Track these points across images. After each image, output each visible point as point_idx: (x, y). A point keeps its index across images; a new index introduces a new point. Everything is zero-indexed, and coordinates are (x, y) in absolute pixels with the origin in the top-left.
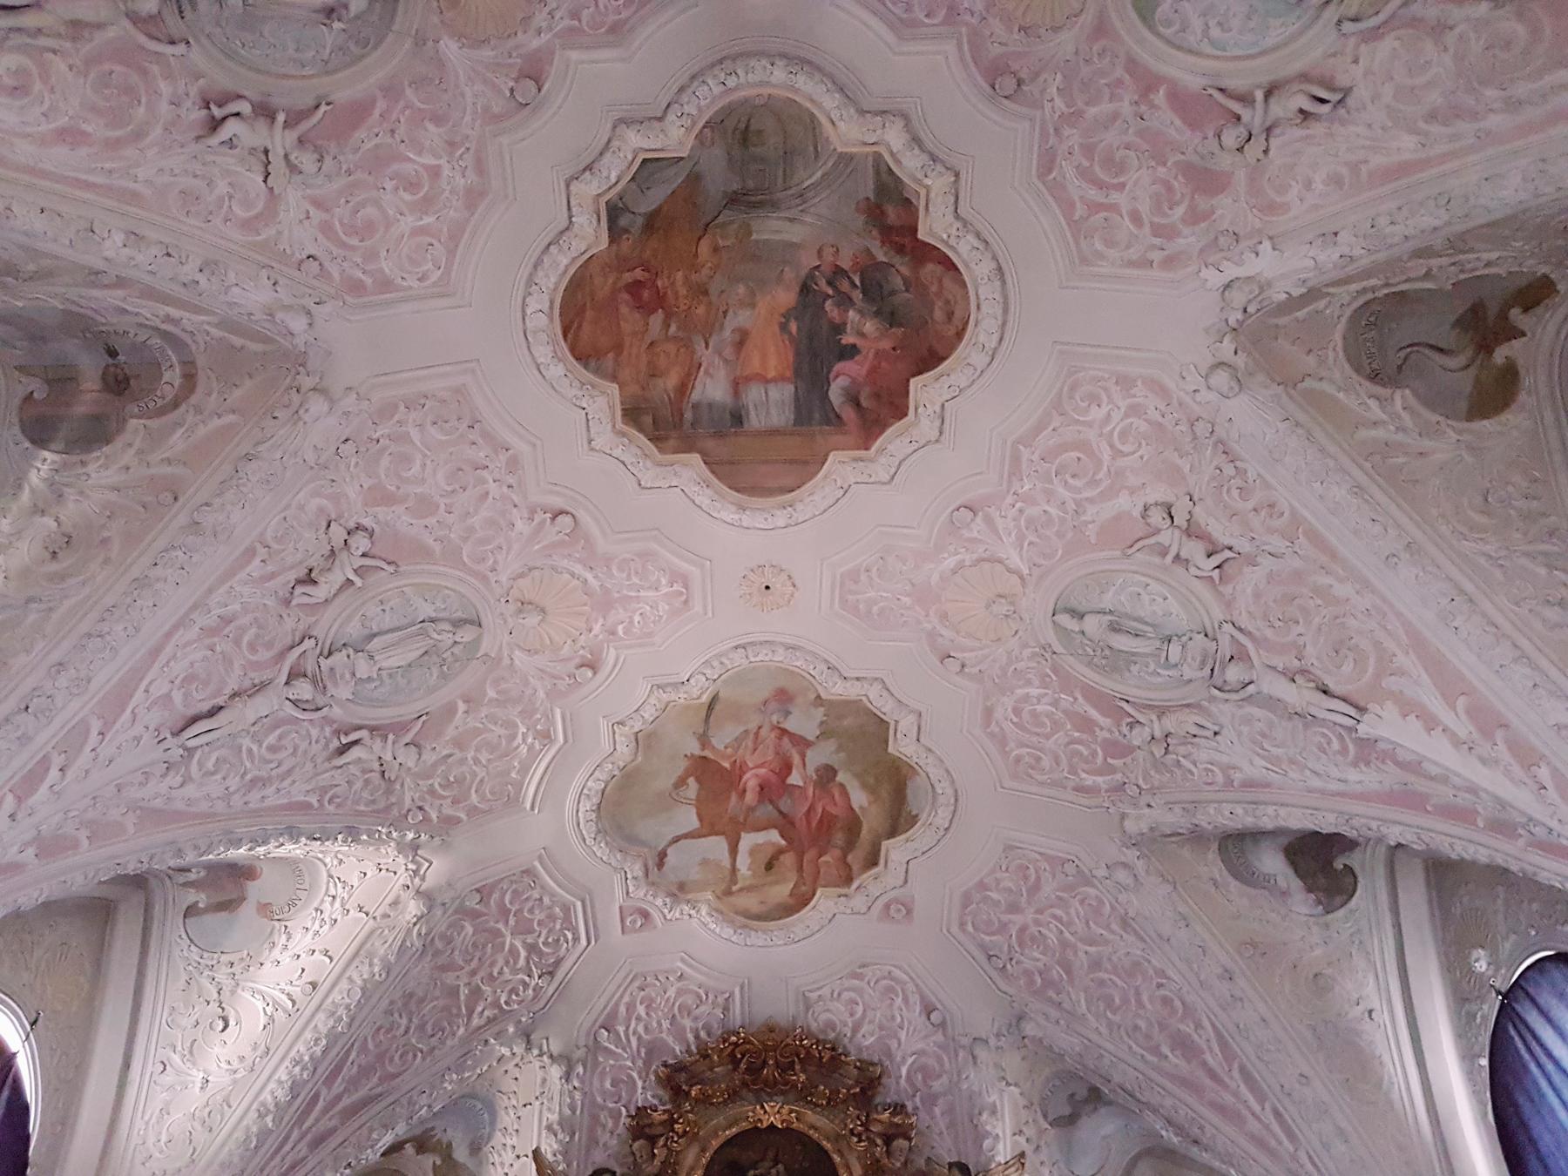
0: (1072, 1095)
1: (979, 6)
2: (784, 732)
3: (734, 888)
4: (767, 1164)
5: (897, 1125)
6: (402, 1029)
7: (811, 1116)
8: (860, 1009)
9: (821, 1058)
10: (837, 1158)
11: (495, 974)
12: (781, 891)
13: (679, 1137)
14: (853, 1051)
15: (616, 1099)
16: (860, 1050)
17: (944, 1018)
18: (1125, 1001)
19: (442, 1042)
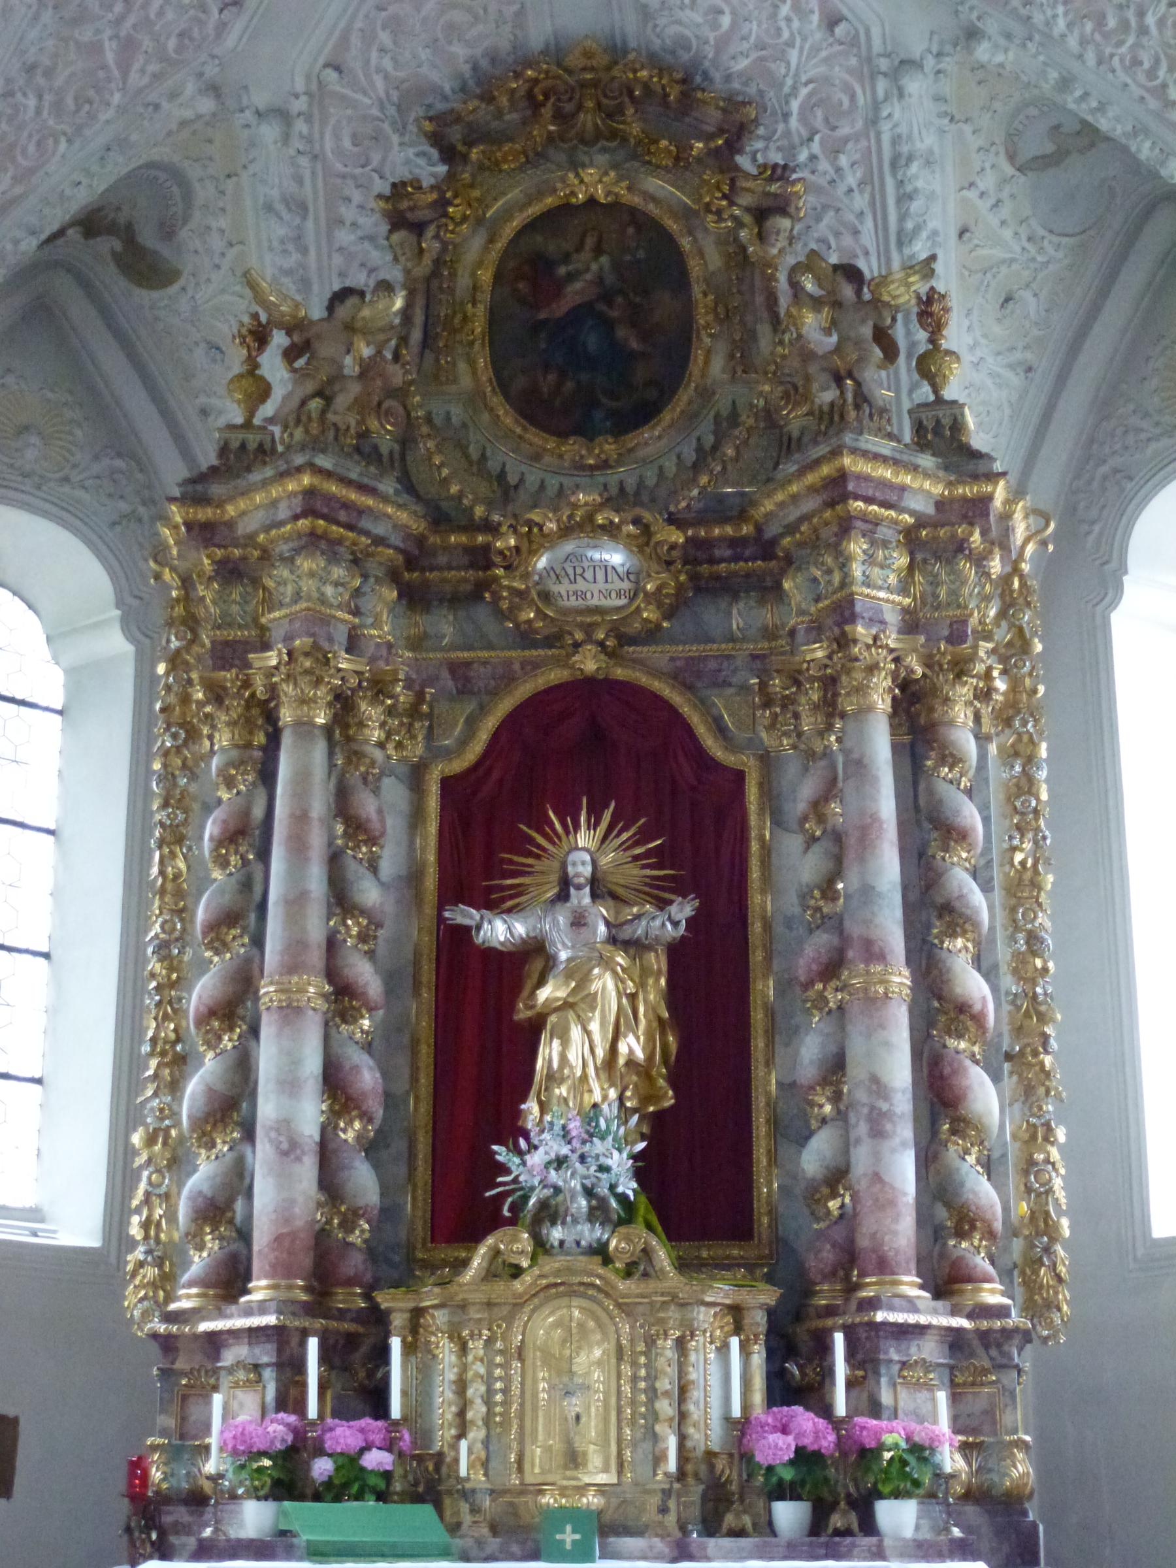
0: (1057, 127)
4: (586, 255)
5: (775, 195)
6: (31, 112)
7: (655, 184)
8: (726, 21)
9: (666, 95)
10: (685, 243)
11: (152, 16)
13: (457, 224)
14: (717, 76)
15: (362, 161)
16: (728, 78)
17: (857, 35)
18: (1124, 26)
19: (92, 116)
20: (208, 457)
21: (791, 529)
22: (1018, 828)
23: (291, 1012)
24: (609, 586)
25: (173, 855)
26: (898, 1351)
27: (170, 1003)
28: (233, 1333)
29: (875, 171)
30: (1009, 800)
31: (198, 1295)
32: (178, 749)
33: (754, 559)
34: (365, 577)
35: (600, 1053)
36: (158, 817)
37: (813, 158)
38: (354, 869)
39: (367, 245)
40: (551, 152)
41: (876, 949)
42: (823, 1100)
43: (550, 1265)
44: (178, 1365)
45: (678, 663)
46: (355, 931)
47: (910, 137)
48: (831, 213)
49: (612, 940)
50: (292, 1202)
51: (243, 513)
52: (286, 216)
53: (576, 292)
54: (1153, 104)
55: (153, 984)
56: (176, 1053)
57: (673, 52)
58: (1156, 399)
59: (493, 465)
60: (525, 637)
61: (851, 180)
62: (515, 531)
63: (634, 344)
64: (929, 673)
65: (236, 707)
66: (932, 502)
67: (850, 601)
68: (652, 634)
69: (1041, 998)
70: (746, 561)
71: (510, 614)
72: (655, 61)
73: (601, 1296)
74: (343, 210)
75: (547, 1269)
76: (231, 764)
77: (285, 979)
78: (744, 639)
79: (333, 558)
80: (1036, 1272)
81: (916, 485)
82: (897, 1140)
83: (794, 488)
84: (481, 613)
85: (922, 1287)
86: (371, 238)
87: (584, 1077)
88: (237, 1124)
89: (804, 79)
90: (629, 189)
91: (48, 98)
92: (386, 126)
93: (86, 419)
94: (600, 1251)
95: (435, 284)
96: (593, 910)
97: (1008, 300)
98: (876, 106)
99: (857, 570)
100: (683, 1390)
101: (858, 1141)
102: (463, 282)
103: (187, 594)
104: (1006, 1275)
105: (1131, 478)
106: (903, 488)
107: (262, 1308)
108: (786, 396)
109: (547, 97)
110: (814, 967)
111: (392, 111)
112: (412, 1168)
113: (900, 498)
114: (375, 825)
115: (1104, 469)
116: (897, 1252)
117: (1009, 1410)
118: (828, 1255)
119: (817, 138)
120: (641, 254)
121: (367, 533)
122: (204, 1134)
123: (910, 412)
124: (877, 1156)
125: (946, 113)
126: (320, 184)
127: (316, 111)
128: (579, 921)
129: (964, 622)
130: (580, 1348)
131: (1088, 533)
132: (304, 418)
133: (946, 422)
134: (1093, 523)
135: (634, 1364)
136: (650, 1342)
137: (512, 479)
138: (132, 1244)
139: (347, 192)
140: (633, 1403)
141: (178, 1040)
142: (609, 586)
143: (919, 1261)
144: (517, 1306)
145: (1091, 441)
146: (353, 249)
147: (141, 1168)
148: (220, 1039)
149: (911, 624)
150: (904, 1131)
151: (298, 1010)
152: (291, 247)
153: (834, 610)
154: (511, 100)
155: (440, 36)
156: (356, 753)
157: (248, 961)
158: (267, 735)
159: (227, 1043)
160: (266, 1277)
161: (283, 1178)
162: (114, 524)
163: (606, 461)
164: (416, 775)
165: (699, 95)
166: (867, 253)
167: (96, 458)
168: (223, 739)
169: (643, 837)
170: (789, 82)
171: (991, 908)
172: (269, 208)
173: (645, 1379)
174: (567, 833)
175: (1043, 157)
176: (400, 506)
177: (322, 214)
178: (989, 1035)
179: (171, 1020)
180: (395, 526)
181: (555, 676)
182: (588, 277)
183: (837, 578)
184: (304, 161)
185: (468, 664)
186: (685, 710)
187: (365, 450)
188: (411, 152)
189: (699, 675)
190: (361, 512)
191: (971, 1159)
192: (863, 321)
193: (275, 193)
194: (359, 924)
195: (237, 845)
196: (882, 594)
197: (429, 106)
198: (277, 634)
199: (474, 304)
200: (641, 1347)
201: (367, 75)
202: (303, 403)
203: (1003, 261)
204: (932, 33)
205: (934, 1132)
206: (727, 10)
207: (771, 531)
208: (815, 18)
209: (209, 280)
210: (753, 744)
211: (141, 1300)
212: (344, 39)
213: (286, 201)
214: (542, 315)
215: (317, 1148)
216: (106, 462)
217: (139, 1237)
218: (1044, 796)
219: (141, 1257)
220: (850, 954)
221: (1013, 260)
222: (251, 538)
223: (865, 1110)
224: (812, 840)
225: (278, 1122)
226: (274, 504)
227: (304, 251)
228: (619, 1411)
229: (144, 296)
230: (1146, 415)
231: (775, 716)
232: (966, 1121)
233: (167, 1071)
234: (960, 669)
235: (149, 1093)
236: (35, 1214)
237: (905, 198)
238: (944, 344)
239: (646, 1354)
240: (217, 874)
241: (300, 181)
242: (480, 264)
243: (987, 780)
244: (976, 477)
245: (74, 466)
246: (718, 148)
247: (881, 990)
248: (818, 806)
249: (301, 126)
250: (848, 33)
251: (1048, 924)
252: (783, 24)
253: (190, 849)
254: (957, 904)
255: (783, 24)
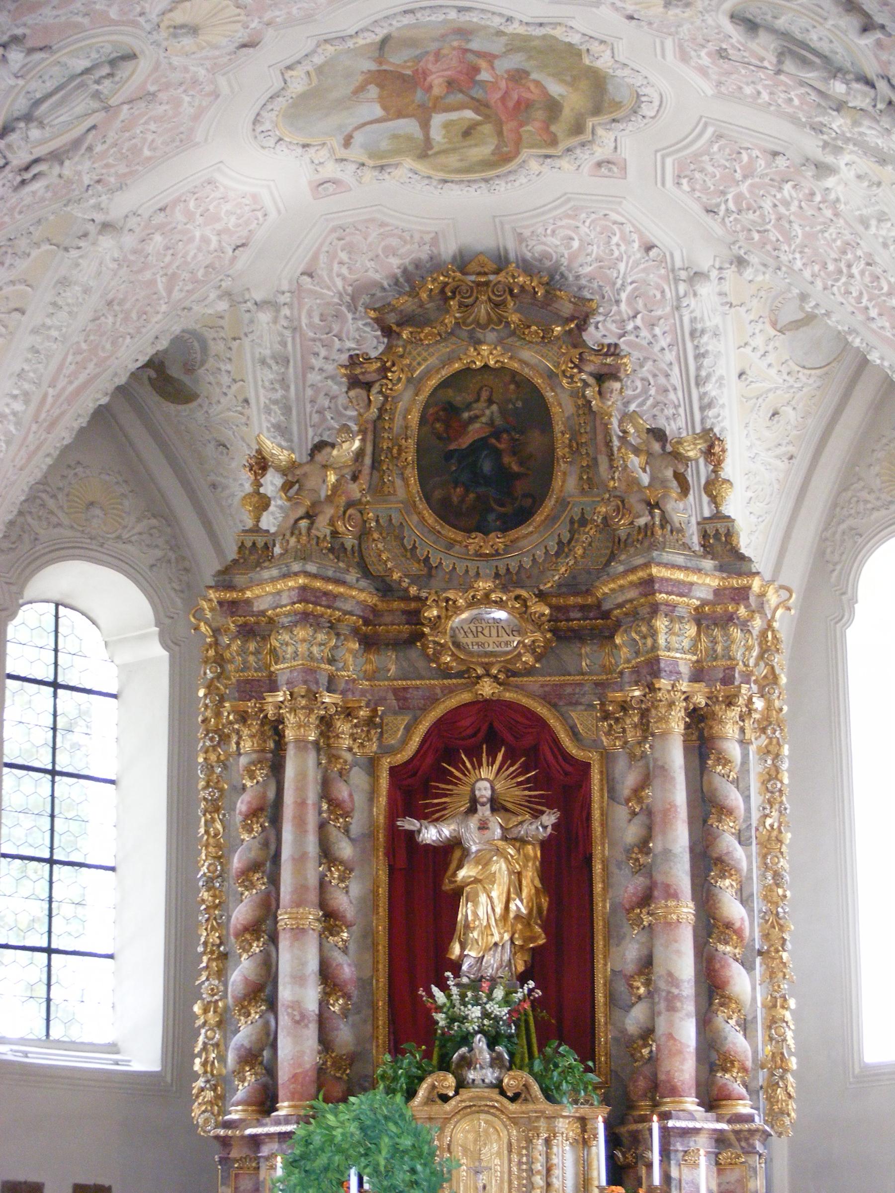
1: (276, 1190)
2: (466, 51)
3: (430, 153)
4: (482, 404)
7: (527, 354)
8: (576, 244)
10: (549, 395)
12: (483, 150)
16: (578, 277)
20: (232, 553)
21: (620, 606)
22: (770, 802)
23: (299, 932)
24: (500, 639)
25: (213, 820)
26: (682, 1144)
27: (215, 919)
28: (269, 1135)
29: (679, 331)
30: (764, 783)
31: (243, 1111)
32: (214, 748)
33: (597, 619)
34: (338, 635)
35: (499, 910)
36: (202, 794)
37: (637, 328)
38: (335, 834)
39: (330, 382)
40: (458, 332)
41: (672, 891)
42: (639, 984)
43: (465, 1094)
44: (232, 1155)
45: (547, 689)
46: (336, 875)
47: (702, 319)
48: (650, 363)
49: (504, 838)
50: (302, 1053)
51: (258, 597)
52: (275, 367)
53: (475, 431)
54: (860, 317)
55: (203, 907)
56: (220, 952)
57: (540, 260)
58: (878, 481)
59: (421, 553)
60: (445, 673)
61: (663, 343)
62: (438, 606)
63: (515, 468)
64: (710, 703)
65: (255, 724)
66: (711, 590)
67: (657, 660)
68: (529, 671)
69: (781, 915)
70: (591, 619)
71: (436, 657)
72: (527, 268)
73: (498, 1113)
74: (313, 361)
75: (464, 1097)
76: (253, 763)
77: (295, 910)
78: (591, 673)
79: (317, 627)
80: (775, 1091)
81: (700, 582)
82: (684, 1012)
83: (621, 582)
84: (413, 654)
85: (699, 1104)
86: (332, 377)
87: (489, 925)
88: (263, 1000)
89: (629, 280)
90: (511, 358)
91: (120, 316)
92: (344, 309)
93: (132, 491)
94: (499, 1086)
95: (380, 424)
96: (492, 819)
97: (773, 415)
98: (679, 299)
99: (662, 641)
100: (549, 1170)
101: (659, 1013)
102: (398, 422)
103: (217, 640)
104: (753, 1093)
105: (861, 535)
106: (692, 584)
107: (287, 1120)
108: (618, 510)
109: (454, 292)
110: (634, 899)
111: (348, 299)
112: (375, 1027)
113: (690, 590)
114: (348, 805)
115: (844, 526)
116: (683, 1083)
117: (752, 1180)
118: (642, 1083)
119: (639, 316)
120: (519, 404)
121: (339, 610)
122: (243, 1007)
123: (698, 523)
124: (671, 1024)
125: (727, 303)
126: (298, 347)
127: (296, 302)
128: (483, 826)
129: (733, 669)
130: (485, 1144)
131: (834, 570)
132: (297, 532)
133: (722, 531)
134: (835, 564)
135: (520, 1155)
136: (529, 1141)
137: (434, 562)
138: (196, 1076)
139: (316, 350)
140: (519, 1178)
141: (221, 944)
142: (500, 639)
143: (698, 1085)
144: (447, 1120)
145: (835, 505)
146: (320, 385)
147: (201, 1027)
148: (251, 946)
149: (698, 675)
150: (690, 1007)
151: (303, 931)
152: (277, 386)
153: (647, 664)
154: (430, 296)
155: (380, 253)
156: (334, 756)
157: (268, 894)
158: (275, 741)
159: (256, 948)
160: (288, 1100)
161: (297, 1039)
162: (153, 566)
163: (497, 551)
164: (372, 765)
165: (558, 293)
166: (675, 389)
167: (139, 520)
168: (247, 745)
169: (525, 769)
170: (619, 282)
171: (749, 857)
172: (263, 362)
173: (526, 1164)
174: (474, 769)
175: (796, 321)
176: (361, 590)
177: (299, 364)
178: (746, 941)
179: (216, 931)
180: (358, 602)
181: (466, 697)
182: (484, 419)
183: (649, 642)
184: (288, 333)
185: (405, 689)
186: (552, 722)
187: (337, 550)
188: (360, 323)
189: (560, 696)
190: (336, 597)
191: (732, 1022)
192: (666, 467)
193: (267, 352)
194: (338, 870)
195: (258, 818)
196: (678, 655)
197: (373, 295)
198: (282, 679)
199: (406, 439)
200: (524, 1144)
201: (331, 278)
202: (297, 521)
203: (770, 390)
204: (715, 256)
205: (711, 1004)
206: (576, 238)
207: (606, 606)
208: (636, 245)
209: (219, 402)
210: (596, 745)
211: (204, 1112)
212: (315, 257)
213: (274, 357)
214: (453, 447)
215: (316, 1018)
216: (145, 522)
217: (200, 1072)
218: (786, 781)
219: (203, 1085)
220: (656, 893)
221: (777, 388)
222: (263, 613)
223: (664, 994)
224: (634, 814)
225: (293, 1002)
226: (279, 593)
227: (287, 388)
228: (510, 1182)
229: (172, 408)
230: (871, 491)
231: (610, 726)
232: (730, 998)
233: (214, 964)
234: (730, 702)
235: (204, 978)
236: (113, 1048)
237: (699, 356)
238: (723, 475)
239: (527, 1148)
240: (245, 836)
241: (284, 344)
242: (408, 411)
243: (748, 771)
244: (740, 574)
245: (125, 527)
246: (571, 330)
247: (674, 917)
248: (637, 792)
249: (286, 311)
250: (659, 255)
251: (787, 866)
252: (614, 248)
253: (224, 815)
254: (725, 858)
255: (614, 248)
